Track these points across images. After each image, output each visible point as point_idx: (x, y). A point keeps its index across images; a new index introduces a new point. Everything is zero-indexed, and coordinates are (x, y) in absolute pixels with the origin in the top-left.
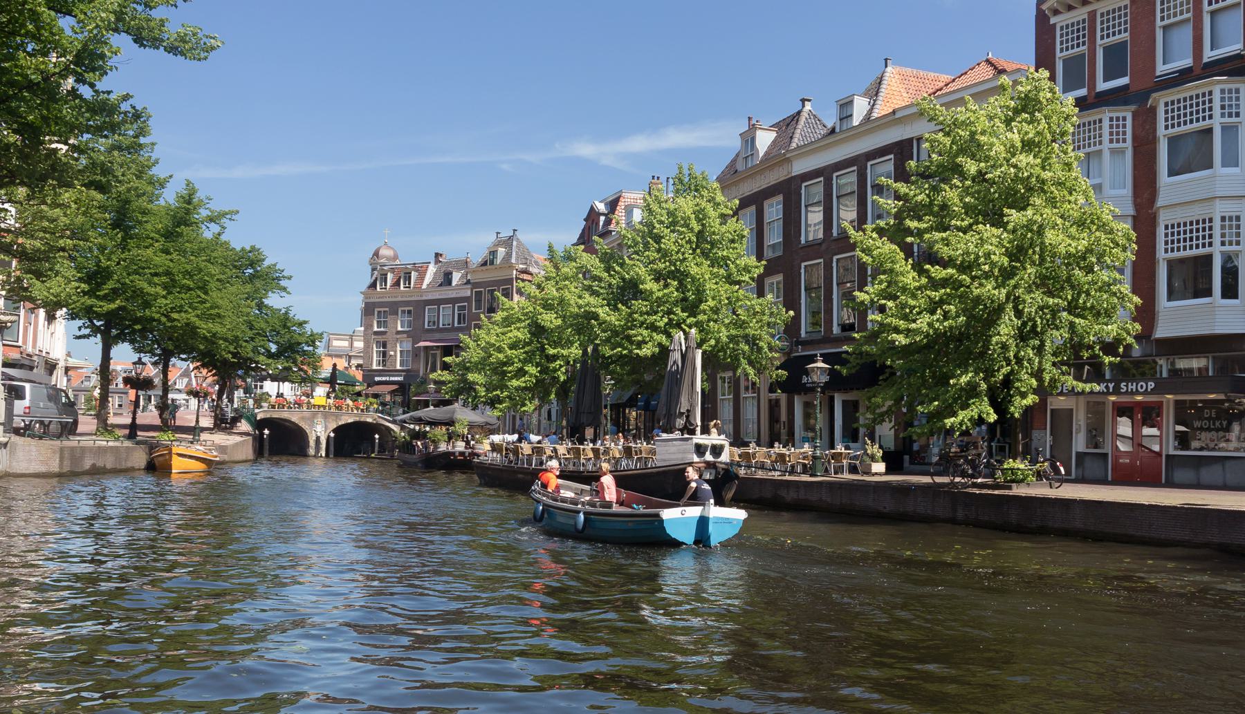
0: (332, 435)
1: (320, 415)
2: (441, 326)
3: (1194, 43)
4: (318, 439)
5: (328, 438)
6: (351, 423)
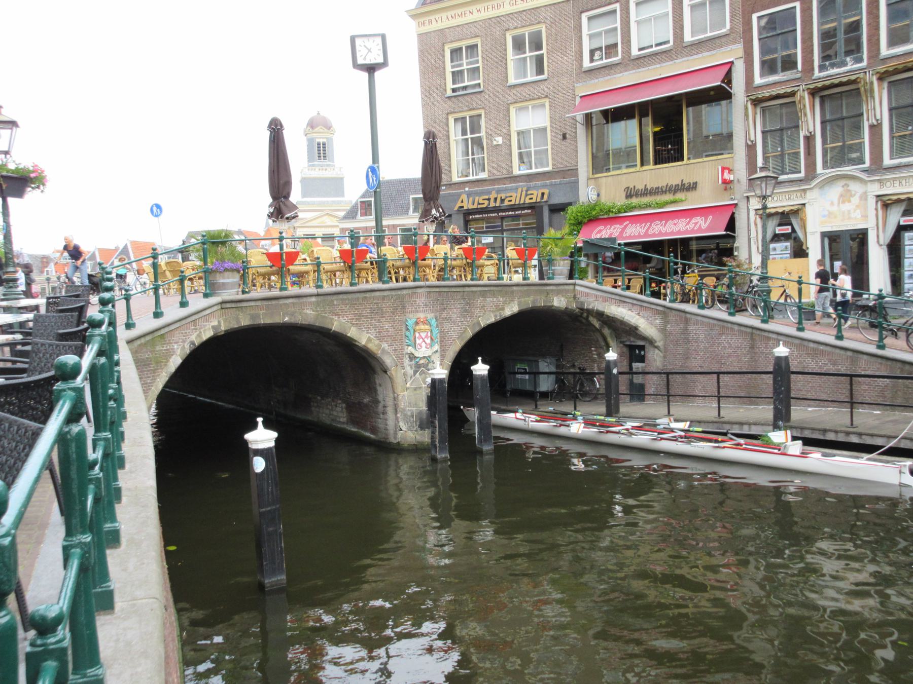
1: (421, 300)
2: (635, 52)
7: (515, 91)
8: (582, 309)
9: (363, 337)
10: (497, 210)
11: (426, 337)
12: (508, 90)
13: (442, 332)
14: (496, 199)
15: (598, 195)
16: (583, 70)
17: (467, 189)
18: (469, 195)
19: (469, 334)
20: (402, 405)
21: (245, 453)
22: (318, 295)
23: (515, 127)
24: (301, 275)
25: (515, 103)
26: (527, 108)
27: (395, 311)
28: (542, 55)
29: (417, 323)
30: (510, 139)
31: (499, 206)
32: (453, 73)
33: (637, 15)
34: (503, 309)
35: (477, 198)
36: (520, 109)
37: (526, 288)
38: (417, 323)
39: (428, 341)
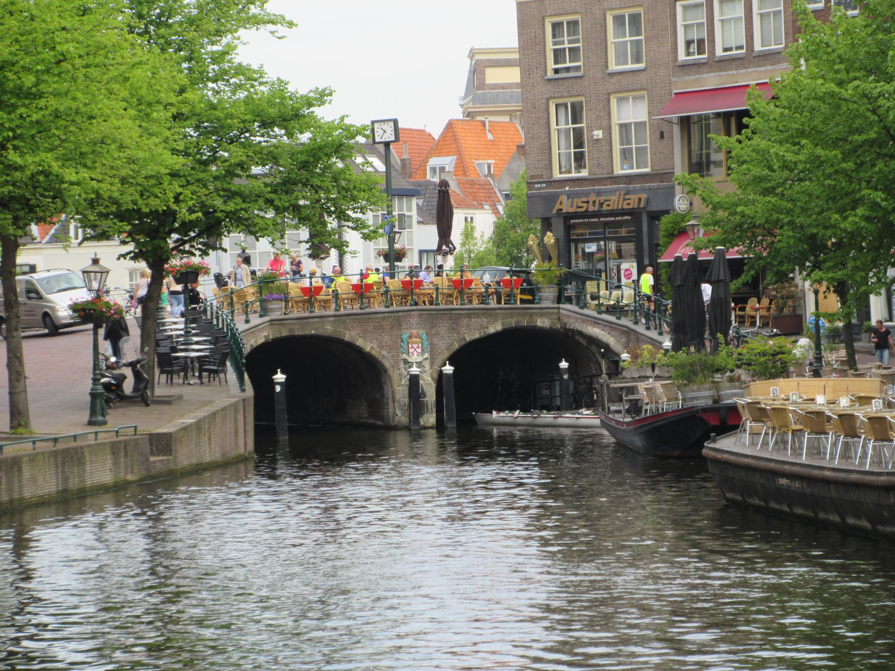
0: (449, 369)
1: (414, 320)
2: (719, 52)
3: (495, 84)
4: (414, 381)
5: (440, 378)
6: (497, 335)
7: (614, 79)
8: (566, 329)
9: (368, 346)
10: (598, 214)
11: (418, 347)
12: (607, 78)
13: (431, 344)
14: (594, 202)
15: (691, 204)
16: (678, 64)
17: (567, 189)
18: (570, 195)
19: (456, 346)
20: (398, 397)
21: (273, 384)
22: (335, 316)
23: (615, 121)
24: (326, 301)
25: (615, 92)
26: (627, 98)
27: (393, 327)
28: (641, 40)
29: (410, 337)
30: (610, 133)
31: (599, 211)
32: (555, 51)
33: (722, 14)
34: (487, 328)
35: (576, 200)
36: (620, 100)
37: (509, 311)
38: (410, 337)
39: (419, 350)
